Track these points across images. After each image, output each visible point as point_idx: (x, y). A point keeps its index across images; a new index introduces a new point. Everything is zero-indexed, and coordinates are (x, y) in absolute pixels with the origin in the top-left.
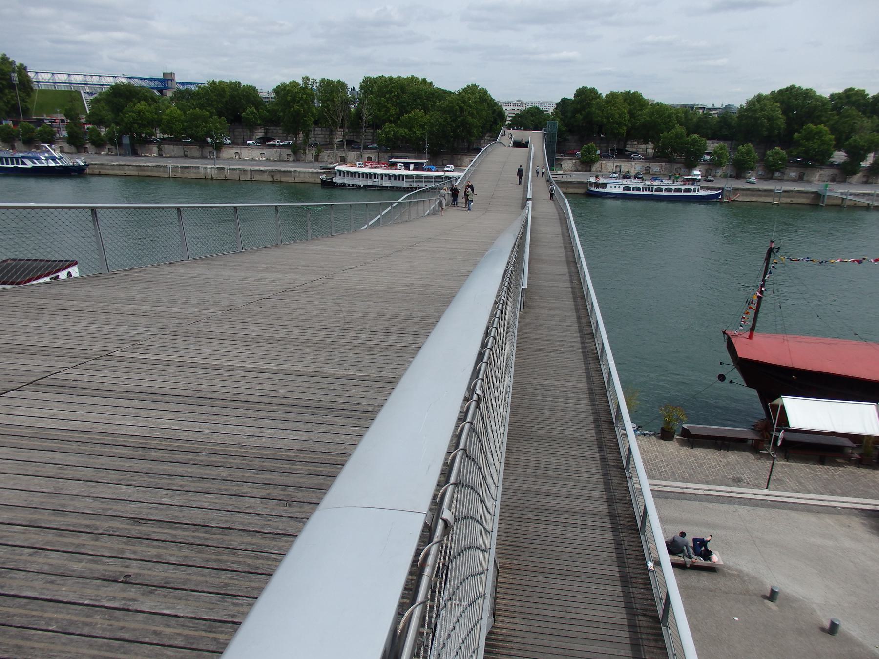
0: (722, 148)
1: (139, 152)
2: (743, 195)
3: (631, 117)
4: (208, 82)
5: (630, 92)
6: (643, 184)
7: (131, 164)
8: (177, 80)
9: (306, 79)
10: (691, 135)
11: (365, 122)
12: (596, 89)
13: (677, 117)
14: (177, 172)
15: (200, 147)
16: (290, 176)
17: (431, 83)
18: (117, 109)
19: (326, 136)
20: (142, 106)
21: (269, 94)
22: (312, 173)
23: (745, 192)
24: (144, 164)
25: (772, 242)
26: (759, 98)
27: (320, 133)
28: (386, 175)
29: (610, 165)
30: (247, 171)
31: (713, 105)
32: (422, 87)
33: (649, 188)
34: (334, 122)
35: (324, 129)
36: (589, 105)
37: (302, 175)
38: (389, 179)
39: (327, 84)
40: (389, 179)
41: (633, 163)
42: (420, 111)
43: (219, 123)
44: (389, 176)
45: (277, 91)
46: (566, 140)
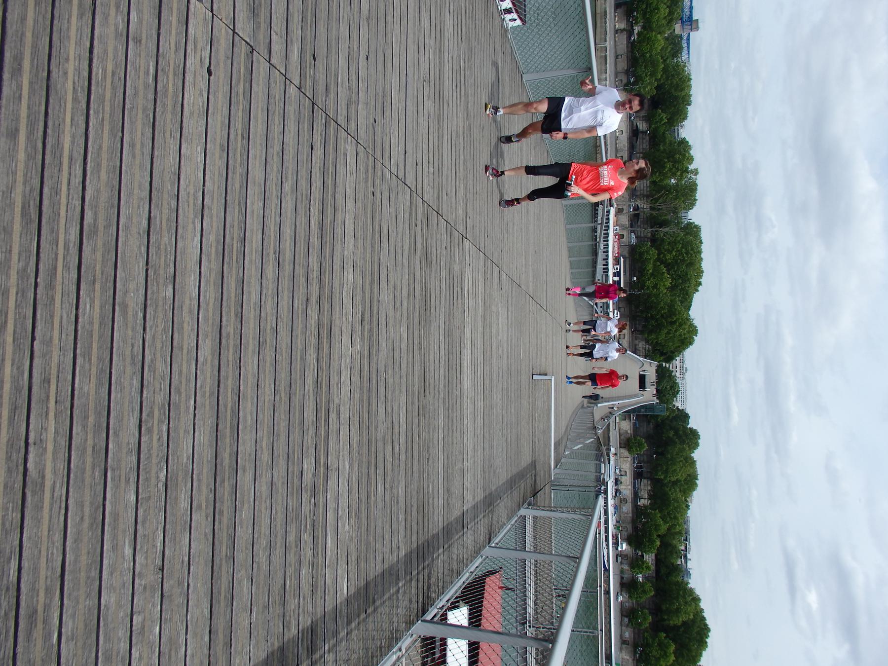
1: (618, 10)
7: (607, 6)
9: (696, 172)
11: (656, 231)
17: (697, 291)
24: (607, 19)
26: (697, 600)
28: (607, 256)
32: (693, 282)
38: (604, 259)
40: (604, 259)
41: (630, 487)
43: (649, 88)
44: (607, 259)
46: (649, 422)
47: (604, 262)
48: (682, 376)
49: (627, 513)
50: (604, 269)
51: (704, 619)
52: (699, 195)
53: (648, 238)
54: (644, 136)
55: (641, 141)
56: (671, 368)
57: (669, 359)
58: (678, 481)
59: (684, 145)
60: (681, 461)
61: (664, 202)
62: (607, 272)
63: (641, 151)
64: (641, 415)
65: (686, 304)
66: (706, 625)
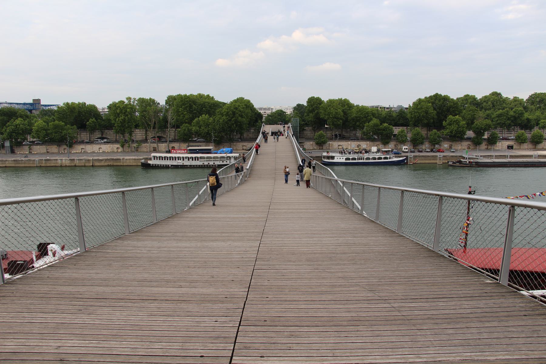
0: (402, 132)
1: (16, 152)
2: (420, 160)
3: (344, 115)
4: (64, 104)
6: (358, 155)
7: (10, 159)
8: (42, 104)
9: (129, 99)
10: (383, 124)
12: (320, 97)
14: (42, 163)
15: (57, 146)
16: (120, 162)
19: (143, 135)
20: (18, 121)
21: (103, 109)
22: (135, 159)
23: (420, 158)
24: (20, 159)
25: (470, 187)
26: (420, 101)
27: (139, 132)
29: (335, 144)
30: (90, 160)
31: (390, 106)
32: (207, 100)
33: (362, 158)
34: (149, 125)
35: (142, 130)
36: (317, 108)
37: (128, 161)
38: (189, 160)
39: (142, 101)
40: (189, 160)
41: (349, 143)
42: (206, 115)
43: (71, 130)
44: (189, 158)
45: (109, 107)
46: (304, 130)
47: (191, 160)
48: (270, 109)
49: (367, 145)
51: (430, 97)
52: (147, 97)
53: (176, 130)
54: (105, 133)
55: (108, 135)
56: (266, 116)
57: (260, 116)
58: (343, 111)
59: (113, 107)
60: (330, 109)
61: (150, 121)
62: (198, 158)
63: (115, 135)
64: (299, 135)
65: (221, 105)
66: (434, 96)
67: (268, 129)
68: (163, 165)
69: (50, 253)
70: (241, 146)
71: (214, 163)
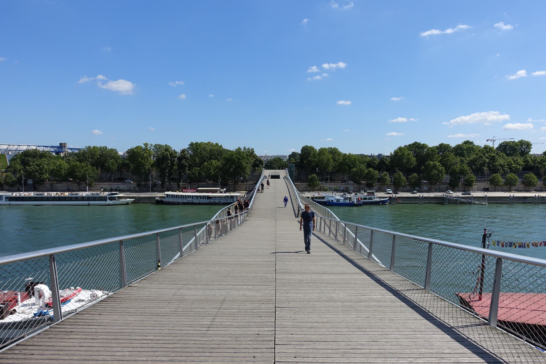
5: (331, 148)
8: (68, 147)
9: (146, 145)
13: (359, 160)
17: (221, 146)
18: (24, 163)
26: (400, 149)
28: (195, 196)
31: (371, 154)
38: (197, 198)
40: (197, 198)
47: (199, 198)
50: (203, 198)
67: (266, 173)
68: (175, 202)
69: (36, 294)
70: (244, 188)
71: (219, 201)
